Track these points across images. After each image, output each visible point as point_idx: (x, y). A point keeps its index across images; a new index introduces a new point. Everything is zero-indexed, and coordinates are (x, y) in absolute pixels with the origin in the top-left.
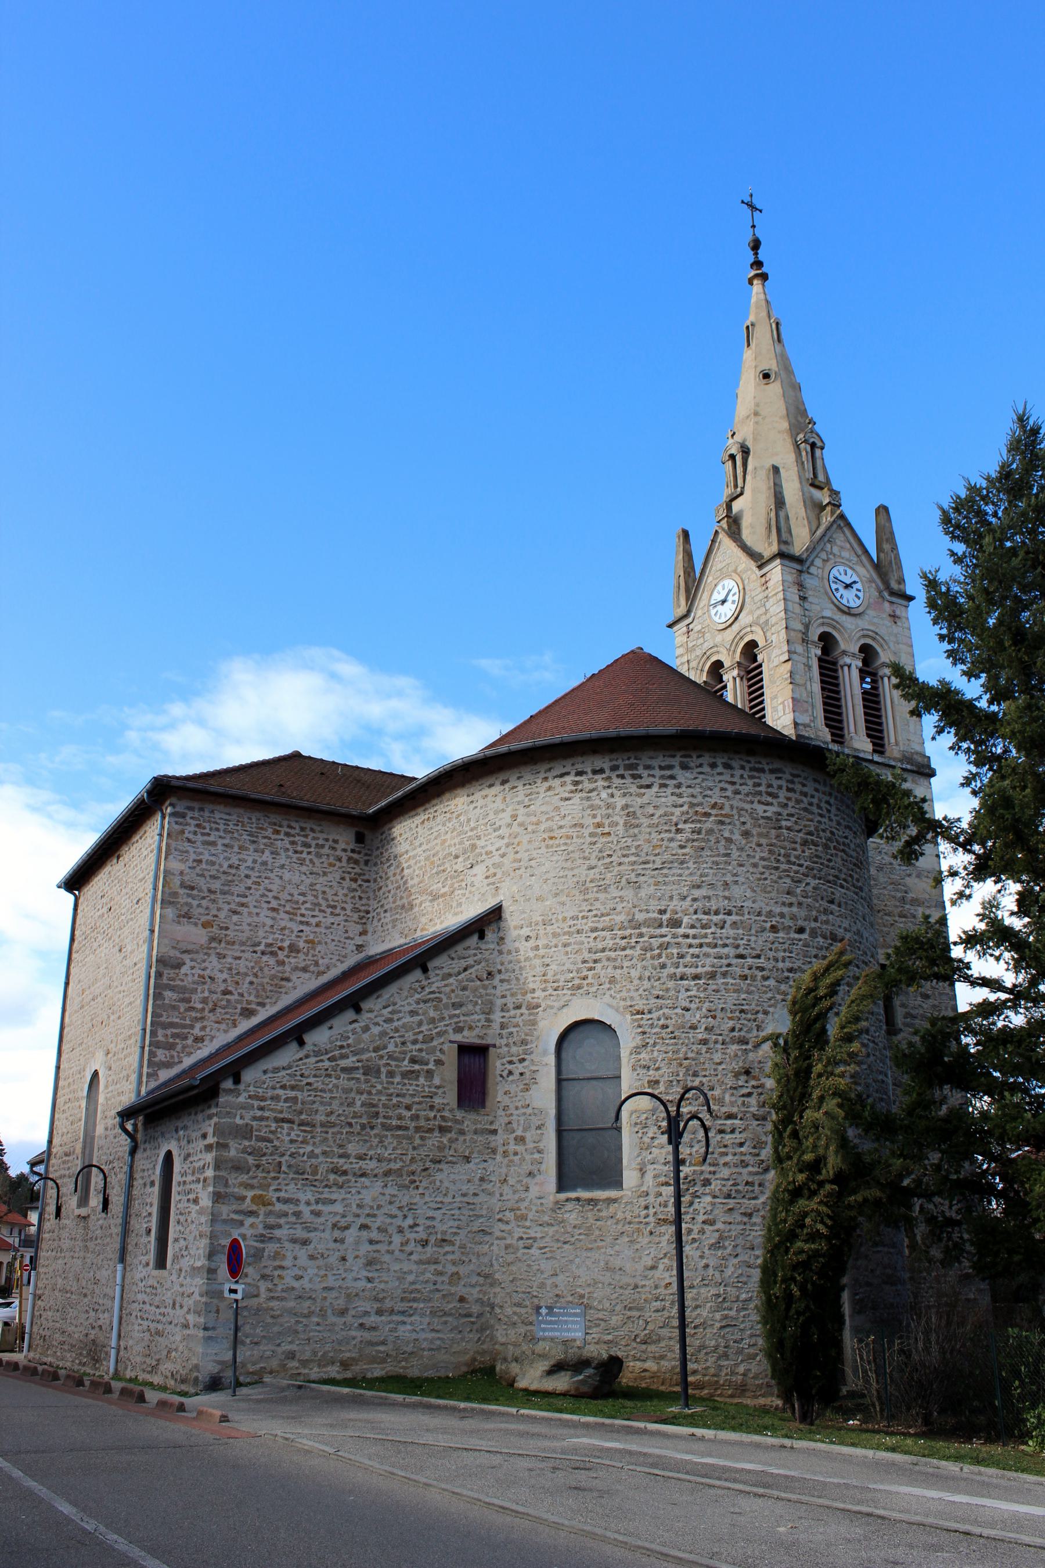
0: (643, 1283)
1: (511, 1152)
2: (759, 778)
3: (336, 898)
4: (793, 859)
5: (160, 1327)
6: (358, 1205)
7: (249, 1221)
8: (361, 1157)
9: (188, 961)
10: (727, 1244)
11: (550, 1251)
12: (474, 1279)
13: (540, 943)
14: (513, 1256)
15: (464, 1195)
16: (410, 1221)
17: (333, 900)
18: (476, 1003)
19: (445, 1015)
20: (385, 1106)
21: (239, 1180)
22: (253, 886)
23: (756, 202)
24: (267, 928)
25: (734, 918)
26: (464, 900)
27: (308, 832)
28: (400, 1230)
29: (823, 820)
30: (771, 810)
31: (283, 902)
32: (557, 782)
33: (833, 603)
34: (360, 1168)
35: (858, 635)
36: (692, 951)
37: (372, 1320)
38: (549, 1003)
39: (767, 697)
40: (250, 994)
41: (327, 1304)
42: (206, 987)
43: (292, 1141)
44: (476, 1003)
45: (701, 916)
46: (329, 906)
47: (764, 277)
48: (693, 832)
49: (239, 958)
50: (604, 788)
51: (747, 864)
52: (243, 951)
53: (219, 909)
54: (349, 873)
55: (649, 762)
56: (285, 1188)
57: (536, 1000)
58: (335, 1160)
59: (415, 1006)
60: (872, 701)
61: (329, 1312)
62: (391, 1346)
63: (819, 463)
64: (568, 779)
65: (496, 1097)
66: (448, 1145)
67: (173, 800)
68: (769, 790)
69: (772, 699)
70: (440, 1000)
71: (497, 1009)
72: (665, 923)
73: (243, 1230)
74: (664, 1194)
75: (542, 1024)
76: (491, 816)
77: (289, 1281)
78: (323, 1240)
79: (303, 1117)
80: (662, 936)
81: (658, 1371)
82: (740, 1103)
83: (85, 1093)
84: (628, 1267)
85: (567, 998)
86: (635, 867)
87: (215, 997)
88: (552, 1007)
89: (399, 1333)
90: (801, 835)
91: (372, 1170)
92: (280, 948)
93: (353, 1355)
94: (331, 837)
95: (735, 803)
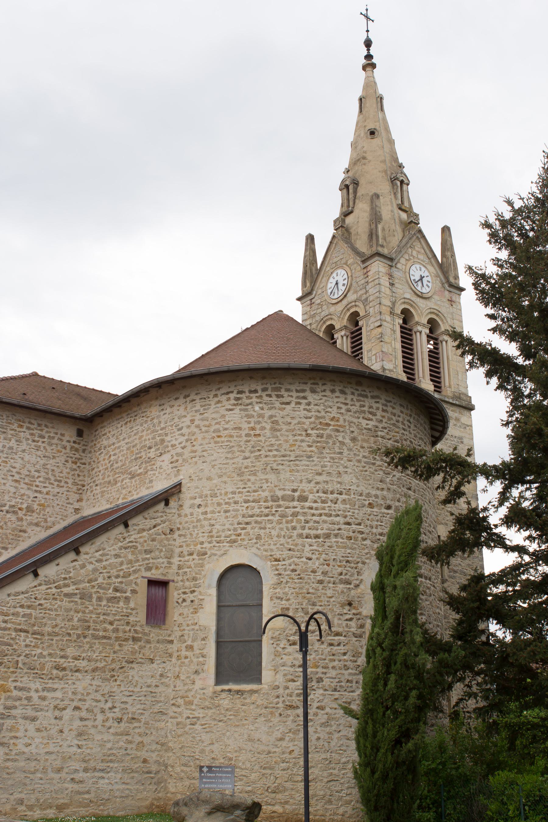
0: (274, 750)
2: (364, 401)
3: (61, 475)
6: (73, 693)
10: (333, 723)
11: (209, 727)
12: (154, 747)
13: (209, 509)
14: (182, 730)
15: (149, 686)
16: (109, 705)
17: (59, 476)
18: (161, 551)
19: (140, 558)
23: (370, 15)
24: (11, 494)
26: (154, 478)
27: (43, 427)
28: (103, 711)
29: (405, 433)
30: (371, 424)
31: (23, 476)
32: (224, 397)
33: (411, 289)
34: (76, 666)
35: (427, 312)
36: (315, 518)
38: (213, 552)
39: (364, 350)
41: (48, 764)
43: (26, 646)
44: (161, 551)
48: (318, 436)
50: (257, 403)
51: (354, 460)
54: (71, 458)
55: (289, 387)
56: (20, 679)
57: (204, 550)
58: (58, 660)
59: (118, 551)
60: (434, 357)
62: (93, 795)
63: (405, 194)
64: (232, 396)
65: (173, 617)
66: (138, 650)
68: (370, 410)
69: (368, 352)
70: (136, 548)
72: (296, 498)
74: (290, 687)
76: (176, 420)
78: (46, 718)
80: (294, 507)
82: (344, 625)
84: (264, 738)
85: (227, 548)
86: (277, 459)
88: (215, 555)
90: (390, 442)
91: (84, 667)
92: (20, 509)
93: (66, 801)
95: (347, 418)
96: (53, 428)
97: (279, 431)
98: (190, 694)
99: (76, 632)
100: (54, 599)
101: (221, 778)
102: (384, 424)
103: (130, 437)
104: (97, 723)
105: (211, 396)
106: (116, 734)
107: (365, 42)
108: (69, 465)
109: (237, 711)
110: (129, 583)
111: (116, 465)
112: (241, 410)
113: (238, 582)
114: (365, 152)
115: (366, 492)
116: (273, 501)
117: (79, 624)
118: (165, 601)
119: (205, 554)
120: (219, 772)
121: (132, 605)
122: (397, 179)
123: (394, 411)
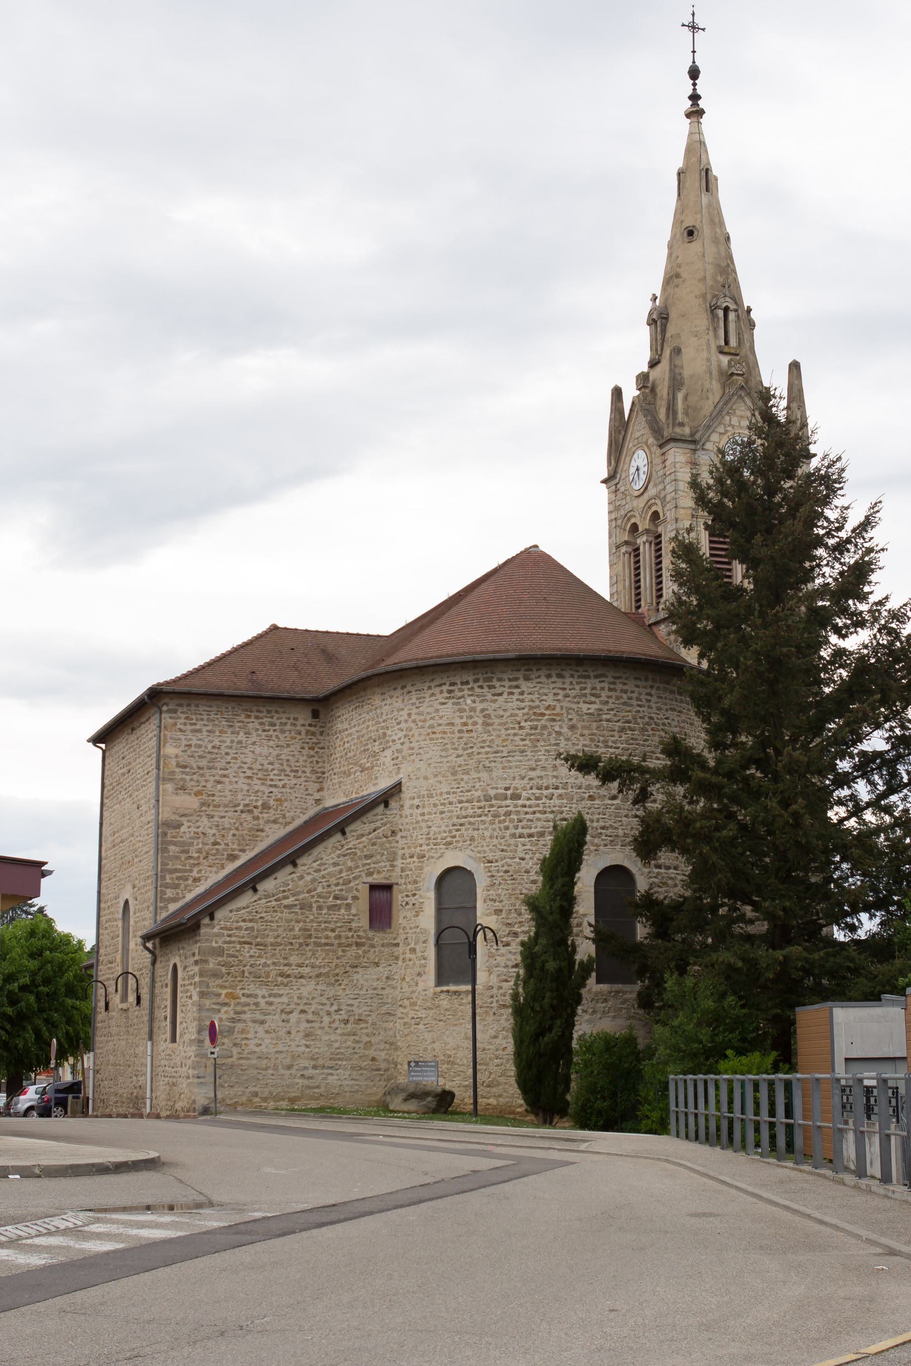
1: (407, 959)
2: (585, 683)
3: (298, 764)
4: (610, 744)
5: (174, 1080)
6: (298, 997)
7: (225, 1009)
8: (299, 966)
12: (382, 1046)
15: (375, 989)
16: (335, 1007)
18: (383, 854)
20: (315, 930)
21: (217, 983)
22: (233, 761)
25: (560, 791)
28: (329, 1014)
31: (255, 771)
32: (437, 690)
36: (528, 816)
37: (310, 1072)
40: (233, 843)
42: (200, 840)
43: (251, 956)
44: (383, 854)
46: (292, 771)
49: (224, 817)
50: (469, 696)
52: (227, 811)
53: (206, 781)
54: (308, 743)
58: (281, 968)
61: (280, 1067)
64: (445, 688)
67: (167, 700)
68: (593, 692)
70: (355, 854)
71: (399, 857)
72: (509, 797)
73: (217, 1016)
75: (426, 869)
77: (252, 1047)
78: (274, 1021)
79: (258, 940)
80: (507, 806)
81: (498, 1105)
83: (120, 916)
85: (443, 851)
87: (207, 847)
88: (433, 857)
89: (329, 1081)
90: (619, 724)
92: (255, 807)
95: (565, 704)
96: (284, 712)
97: (491, 725)
98: (414, 996)
99: (298, 941)
100: (274, 911)
101: (426, 1071)
102: (610, 705)
103: (359, 725)
104: (323, 1025)
105: (426, 688)
106: (343, 1034)
107: (689, 72)
108: (305, 752)
109: (455, 1011)
111: (349, 755)
112: (453, 704)
113: (454, 884)
114: (679, 266)
116: (486, 800)
117: (300, 933)
118: (389, 905)
119: (424, 856)
120: (424, 1066)
121: (354, 911)
122: (718, 307)
123: (625, 687)
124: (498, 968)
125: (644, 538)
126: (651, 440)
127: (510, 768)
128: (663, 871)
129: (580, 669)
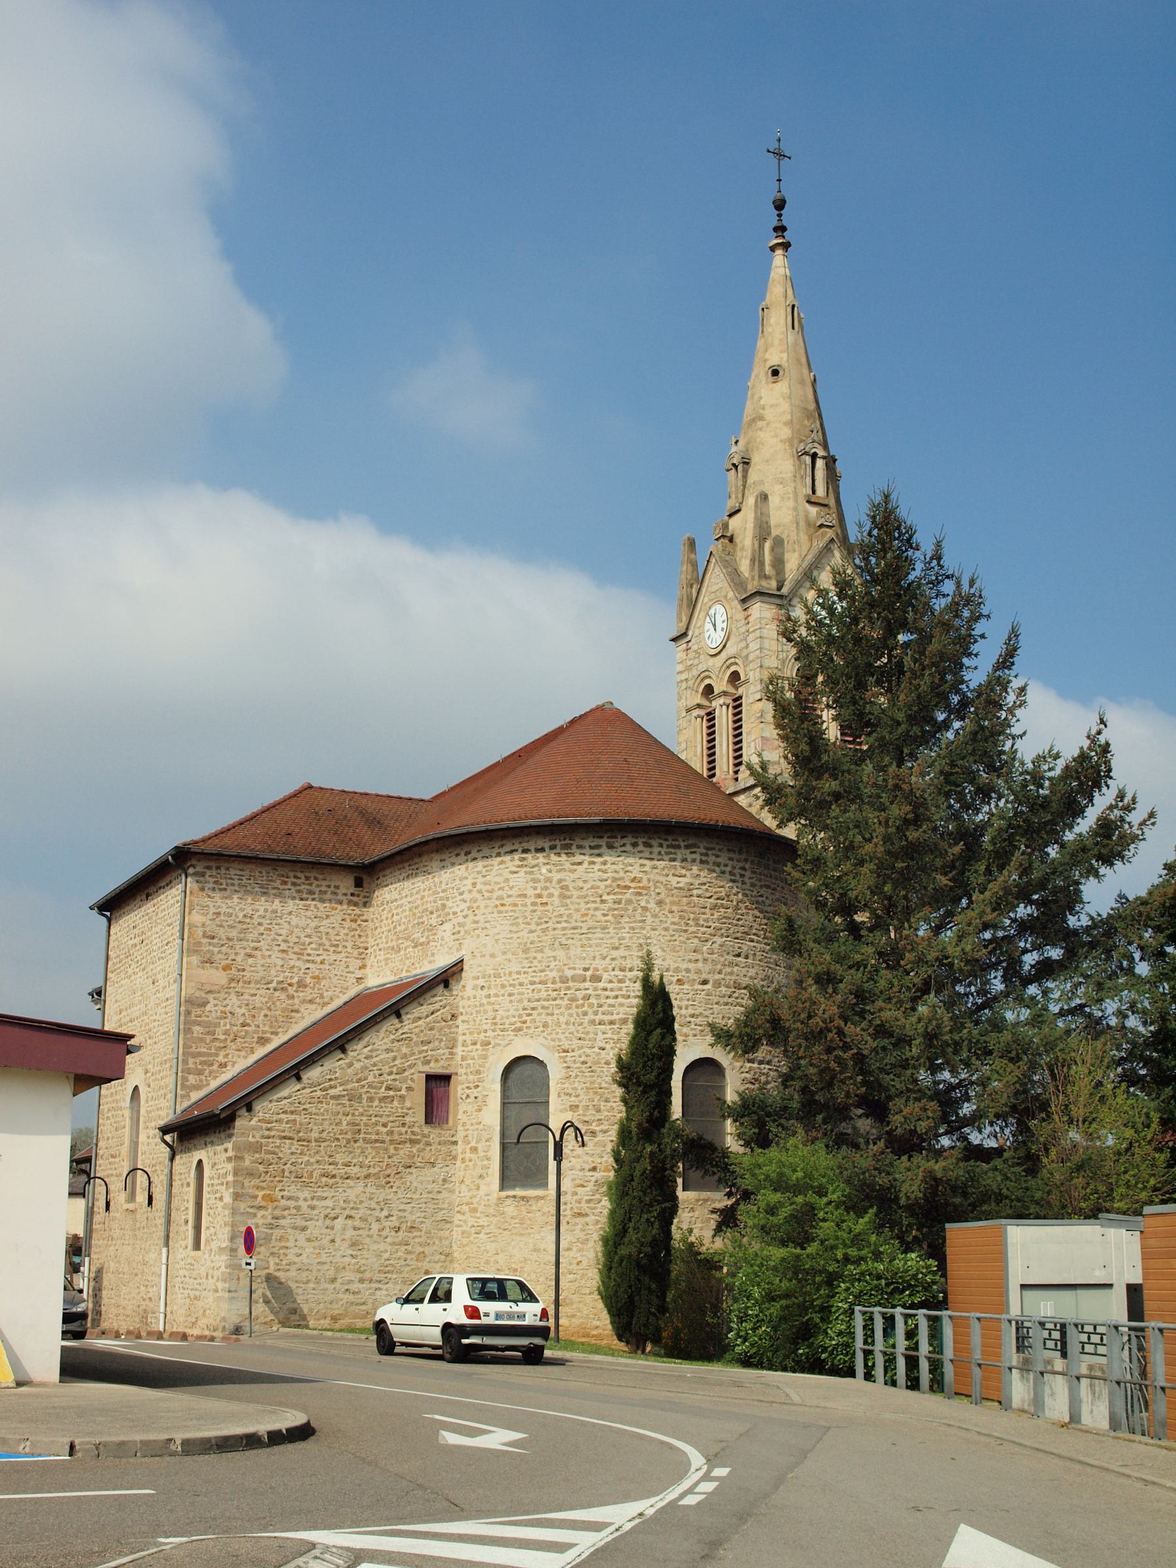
4: (701, 922)
5: (197, 1293)
7: (262, 1212)
9: (211, 1000)
12: (437, 1257)
15: (429, 1193)
16: (385, 1213)
18: (441, 1040)
20: (366, 1125)
24: (279, 968)
27: (312, 880)
30: (683, 881)
31: (291, 944)
32: (507, 858)
36: (610, 1001)
37: (355, 1286)
43: (292, 1153)
44: (441, 1040)
45: (617, 972)
46: (332, 945)
47: (786, 246)
58: (326, 1167)
62: (370, 1306)
64: (517, 856)
67: (194, 862)
71: (460, 1044)
73: (254, 1221)
77: (292, 1257)
78: (316, 1228)
85: (511, 1037)
90: (711, 900)
92: (290, 985)
94: (333, 884)
95: (652, 877)
97: (569, 897)
98: (475, 1200)
103: (412, 895)
106: (393, 1244)
108: (347, 924)
109: (522, 1219)
110: (405, 1080)
111: (399, 928)
113: (522, 1074)
115: (673, 966)
123: (719, 860)
124: (588, 1172)
125: (721, 701)
126: (731, 594)
127: (590, 946)
128: (756, 1065)
129: (670, 838)
